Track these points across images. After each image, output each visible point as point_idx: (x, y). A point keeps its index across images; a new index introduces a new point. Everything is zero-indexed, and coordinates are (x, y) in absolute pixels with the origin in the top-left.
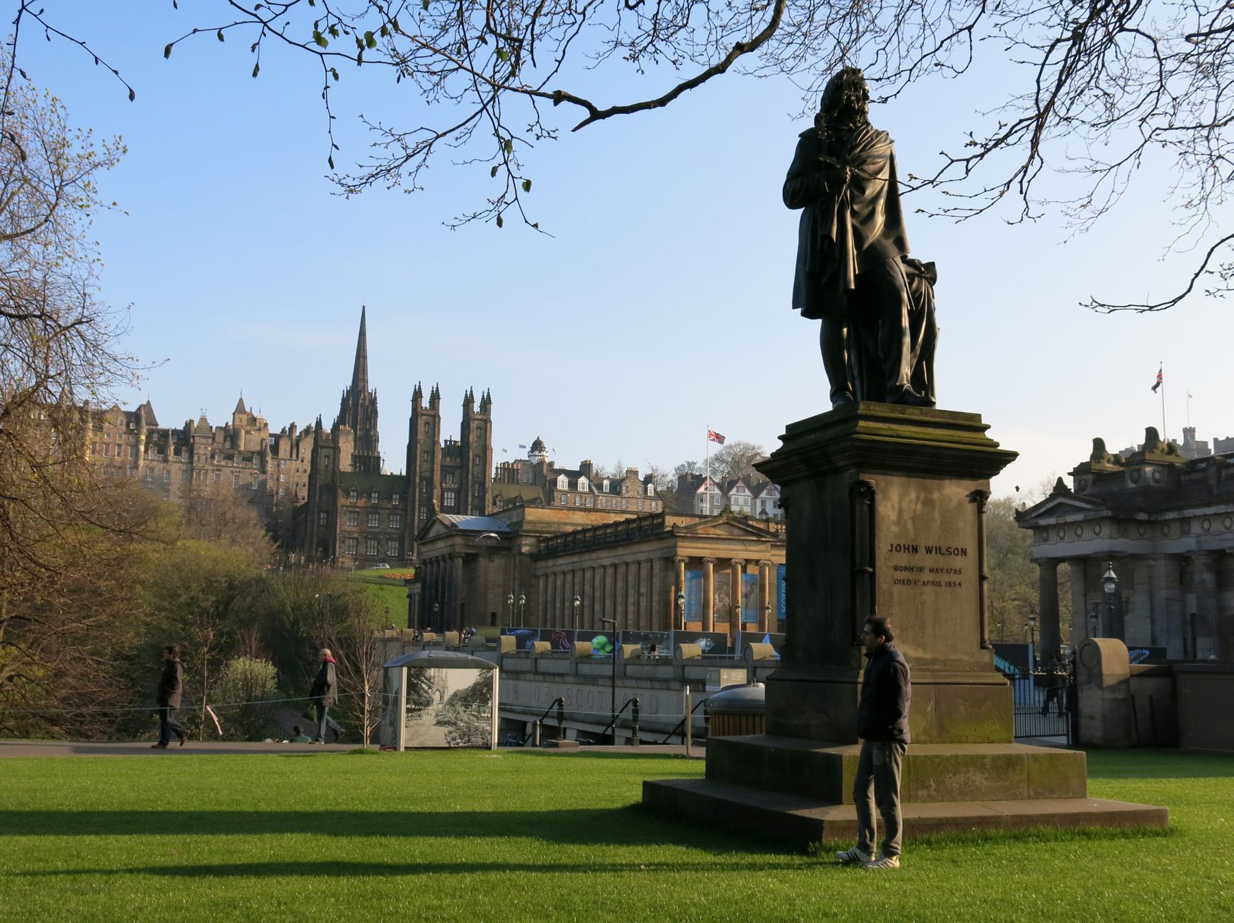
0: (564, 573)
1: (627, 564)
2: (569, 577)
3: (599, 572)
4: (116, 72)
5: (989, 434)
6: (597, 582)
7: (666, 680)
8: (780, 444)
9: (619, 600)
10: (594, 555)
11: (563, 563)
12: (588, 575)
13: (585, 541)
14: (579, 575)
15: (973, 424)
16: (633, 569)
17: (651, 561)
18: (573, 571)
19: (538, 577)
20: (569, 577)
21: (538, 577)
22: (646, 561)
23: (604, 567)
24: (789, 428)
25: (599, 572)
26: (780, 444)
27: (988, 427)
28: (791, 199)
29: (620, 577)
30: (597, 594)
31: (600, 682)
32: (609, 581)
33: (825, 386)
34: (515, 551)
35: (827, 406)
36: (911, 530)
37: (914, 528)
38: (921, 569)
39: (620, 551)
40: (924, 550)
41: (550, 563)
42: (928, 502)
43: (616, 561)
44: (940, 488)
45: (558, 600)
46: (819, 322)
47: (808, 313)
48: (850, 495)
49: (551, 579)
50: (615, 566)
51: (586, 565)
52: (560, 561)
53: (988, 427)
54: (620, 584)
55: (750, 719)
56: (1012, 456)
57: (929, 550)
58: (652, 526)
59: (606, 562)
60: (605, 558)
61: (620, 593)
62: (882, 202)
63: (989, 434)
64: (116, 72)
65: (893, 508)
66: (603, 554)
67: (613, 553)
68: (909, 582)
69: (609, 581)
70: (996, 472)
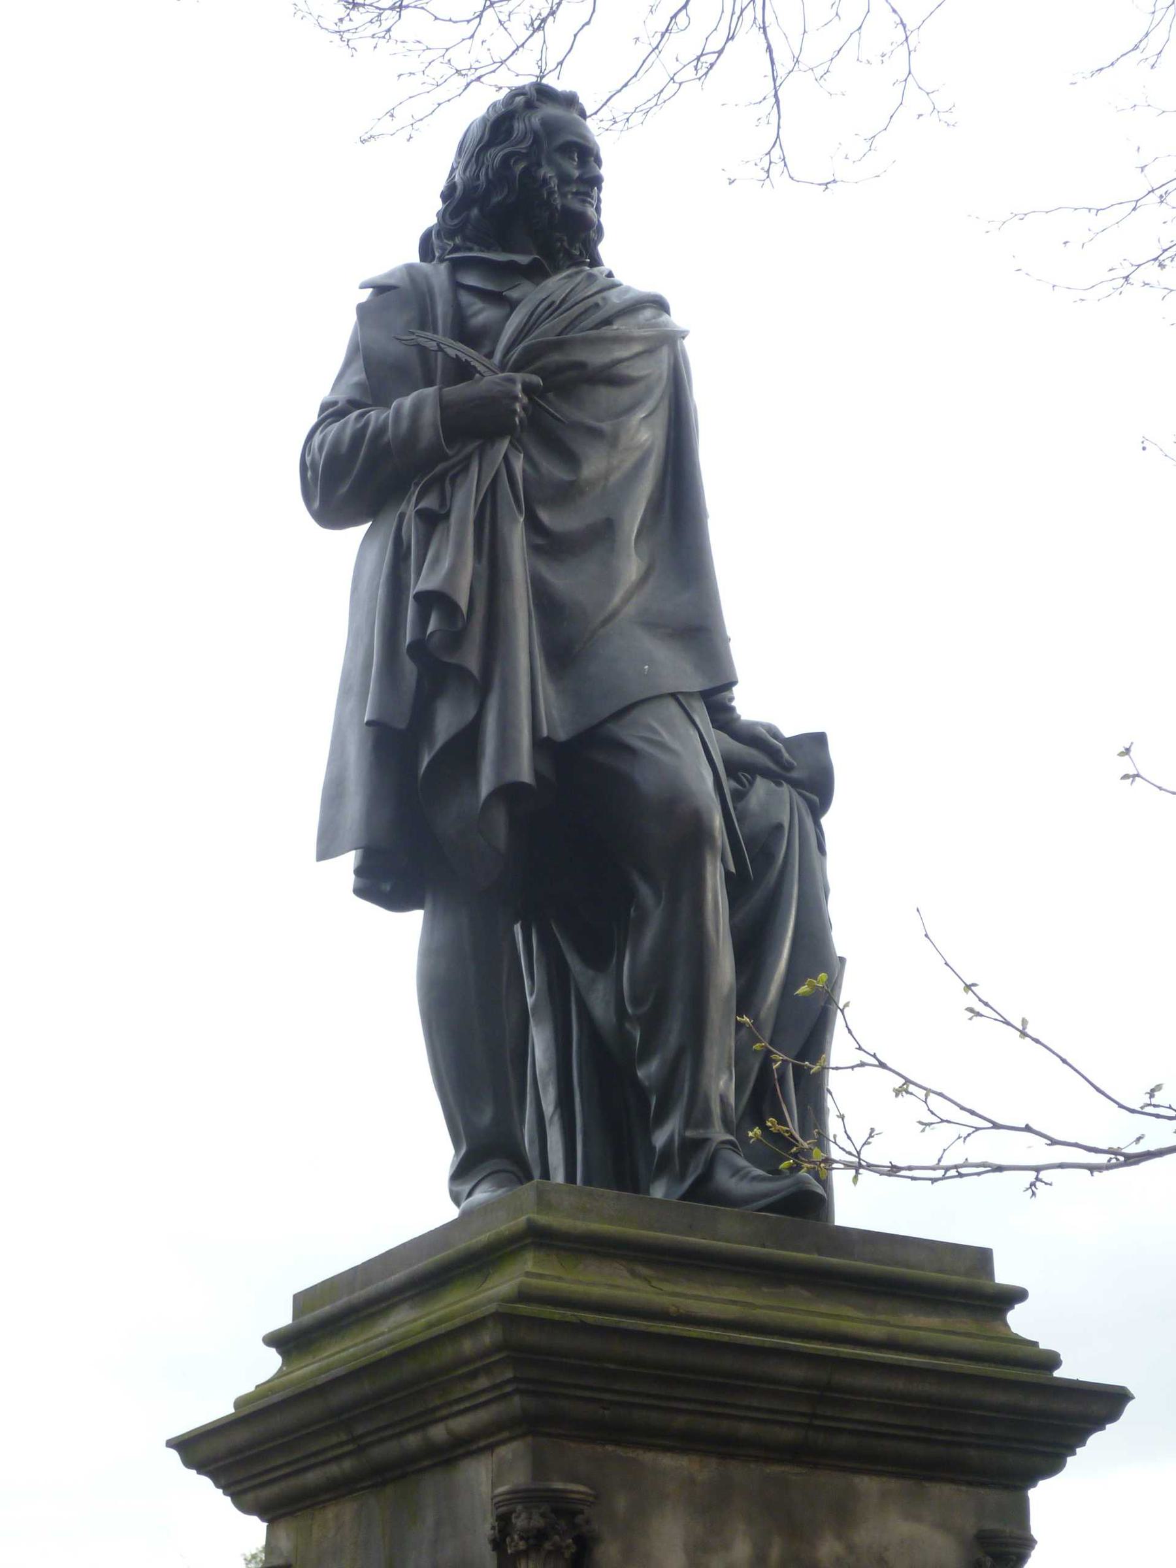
4: (926, 935)
5: (1020, 1321)
8: (268, 1364)
15: (964, 1286)
24: (302, 1301)
26: (271, 1363)
27: (1016, 1296)
28: (348, 476)
33: (440, 1151)
42: (851, 1548)
44: (844, 1515)
46: (415, 919)
47: (384, 882)
48: (498, 1544)
53: (1016, 1296)
56: (1105, 1403)
62: (532, 368)
63: (1019, 1321)
64: (926, 935)
70: (1052, 1464)
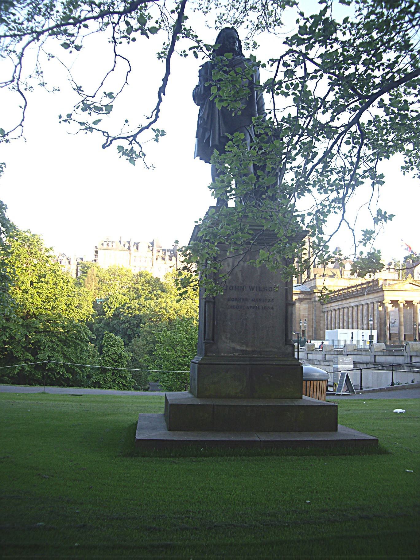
0: (335, 310)
1: (362, 305)
2: (337, 312)
3: (351, 309)
6: (350, 314)
7: (319, 361)
9: (360, 322)
10: (348, 301)
11: (335, 305)
12: (346, 310)
13: (344, 295)
14: (341, 311)
16: (365, 307)
17: (373, 303)
18: (339, 309)
19: (324, 313)
20: (337, 312)
21: (324, 313)
22: (371, 303)
23: (353, 307)
25: (351, 309)
29: (359, 312)
30: (350, 320)
31: (316, 363)
32: (355, 313)
34: (313, 300)
35: (215, 205)
36: (240, 277)
37: (242, 276)
38: (246, 299)
39: (360, 299)
40: (248, 289)
41: (329, 305)
43: (357, 303)
45: (333, 323)
49: (329, 313)
50: (357, 306)
51: (345, 306)
52: (333, 304)
54: (360, 315)
55: (315, 382)
57: (251, 289)
58: (374, 286)
59: (353, 304)
60: (353, 302)
61: (360, 319)
65: (228, 265)
66: (352, 300)
67: (356, 300)
68: (237, 307)
69: (355, 313)
